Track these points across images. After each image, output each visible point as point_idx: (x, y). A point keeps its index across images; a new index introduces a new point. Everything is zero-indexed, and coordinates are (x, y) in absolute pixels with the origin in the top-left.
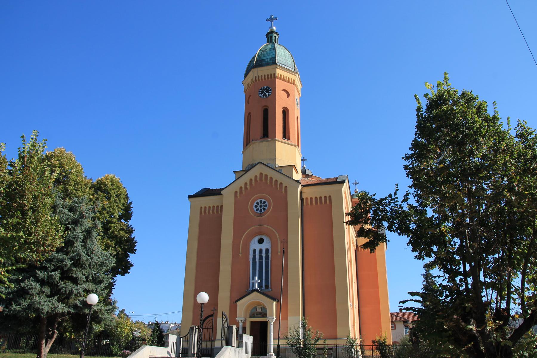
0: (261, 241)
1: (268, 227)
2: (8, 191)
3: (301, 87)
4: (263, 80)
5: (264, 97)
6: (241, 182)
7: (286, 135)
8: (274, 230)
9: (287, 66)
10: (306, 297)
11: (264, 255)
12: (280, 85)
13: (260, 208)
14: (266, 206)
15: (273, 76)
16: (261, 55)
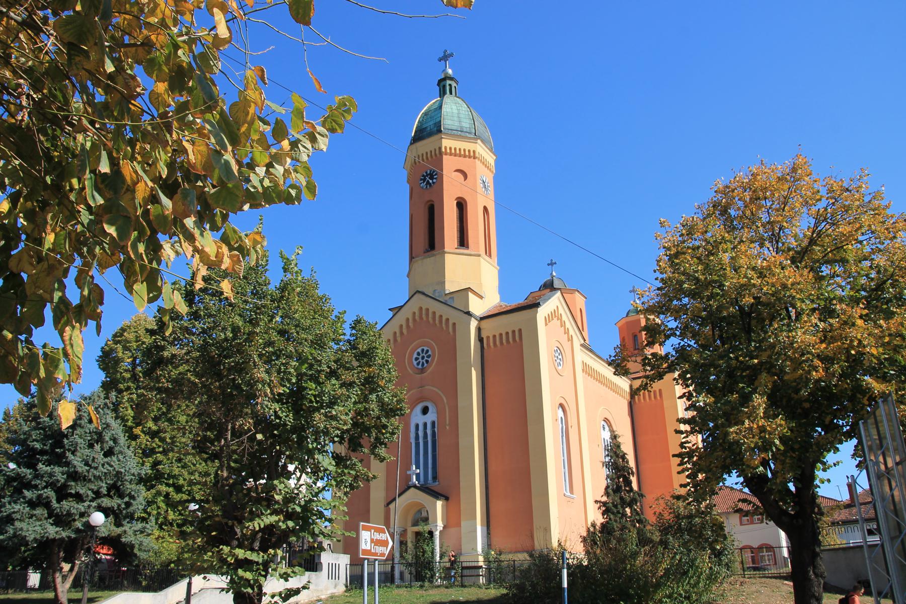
0: (425, 411)
3: (495, 158)
7: (463, 241)
8: (440, 392)
11: (429, 432)
12: (449, 164)
13: (421, 361)
14: (429, 356)
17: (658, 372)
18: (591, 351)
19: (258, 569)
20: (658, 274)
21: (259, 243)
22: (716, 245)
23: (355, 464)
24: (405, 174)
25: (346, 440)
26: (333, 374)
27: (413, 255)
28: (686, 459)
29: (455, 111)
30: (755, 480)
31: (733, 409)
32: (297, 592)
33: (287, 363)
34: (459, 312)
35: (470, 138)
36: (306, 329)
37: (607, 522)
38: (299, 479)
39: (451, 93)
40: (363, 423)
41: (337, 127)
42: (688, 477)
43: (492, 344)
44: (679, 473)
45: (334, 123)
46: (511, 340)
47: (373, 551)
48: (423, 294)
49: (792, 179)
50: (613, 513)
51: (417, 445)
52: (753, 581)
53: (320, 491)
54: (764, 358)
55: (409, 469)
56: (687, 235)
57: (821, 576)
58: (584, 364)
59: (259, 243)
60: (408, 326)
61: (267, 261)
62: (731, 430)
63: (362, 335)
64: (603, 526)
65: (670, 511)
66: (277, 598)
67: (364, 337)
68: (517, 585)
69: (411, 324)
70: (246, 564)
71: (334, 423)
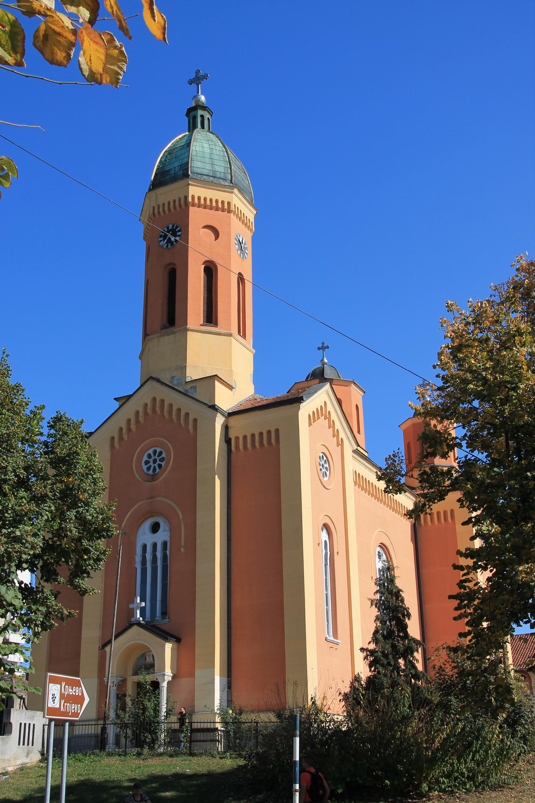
0: (155, 528)
2: (488, 657)
3: (255, 212)
4: (167, 212)
5: (167, 246)
6: (120, 421)
8: (175, 506)
9: (214, 177)
11: (159, 555)
14: (162, 460)
15: (182, 202)
16: (165, 160)
17: (438, 490)
20: (438, 371)
23: (47, 598)
24: (140, 229)
25: (39, 566)
26: (22, 483)
27: (148, 332)
28: (466, 602)
29: (207, 151)
31: (525, 542)
37: (374, 676)
39: (203, 127)
42: (467, 624)
43: (241, 447)
44: (455, 619)
48: (158, 381)
50: (383, 666)
55: (133, 601)
56: (474, 324)
58: (357, 476)
63: (62, 436)
64: (370, 680)
67: (65, 438)
68: (257, 754)
69: (141, 419)
71: (17, 546)
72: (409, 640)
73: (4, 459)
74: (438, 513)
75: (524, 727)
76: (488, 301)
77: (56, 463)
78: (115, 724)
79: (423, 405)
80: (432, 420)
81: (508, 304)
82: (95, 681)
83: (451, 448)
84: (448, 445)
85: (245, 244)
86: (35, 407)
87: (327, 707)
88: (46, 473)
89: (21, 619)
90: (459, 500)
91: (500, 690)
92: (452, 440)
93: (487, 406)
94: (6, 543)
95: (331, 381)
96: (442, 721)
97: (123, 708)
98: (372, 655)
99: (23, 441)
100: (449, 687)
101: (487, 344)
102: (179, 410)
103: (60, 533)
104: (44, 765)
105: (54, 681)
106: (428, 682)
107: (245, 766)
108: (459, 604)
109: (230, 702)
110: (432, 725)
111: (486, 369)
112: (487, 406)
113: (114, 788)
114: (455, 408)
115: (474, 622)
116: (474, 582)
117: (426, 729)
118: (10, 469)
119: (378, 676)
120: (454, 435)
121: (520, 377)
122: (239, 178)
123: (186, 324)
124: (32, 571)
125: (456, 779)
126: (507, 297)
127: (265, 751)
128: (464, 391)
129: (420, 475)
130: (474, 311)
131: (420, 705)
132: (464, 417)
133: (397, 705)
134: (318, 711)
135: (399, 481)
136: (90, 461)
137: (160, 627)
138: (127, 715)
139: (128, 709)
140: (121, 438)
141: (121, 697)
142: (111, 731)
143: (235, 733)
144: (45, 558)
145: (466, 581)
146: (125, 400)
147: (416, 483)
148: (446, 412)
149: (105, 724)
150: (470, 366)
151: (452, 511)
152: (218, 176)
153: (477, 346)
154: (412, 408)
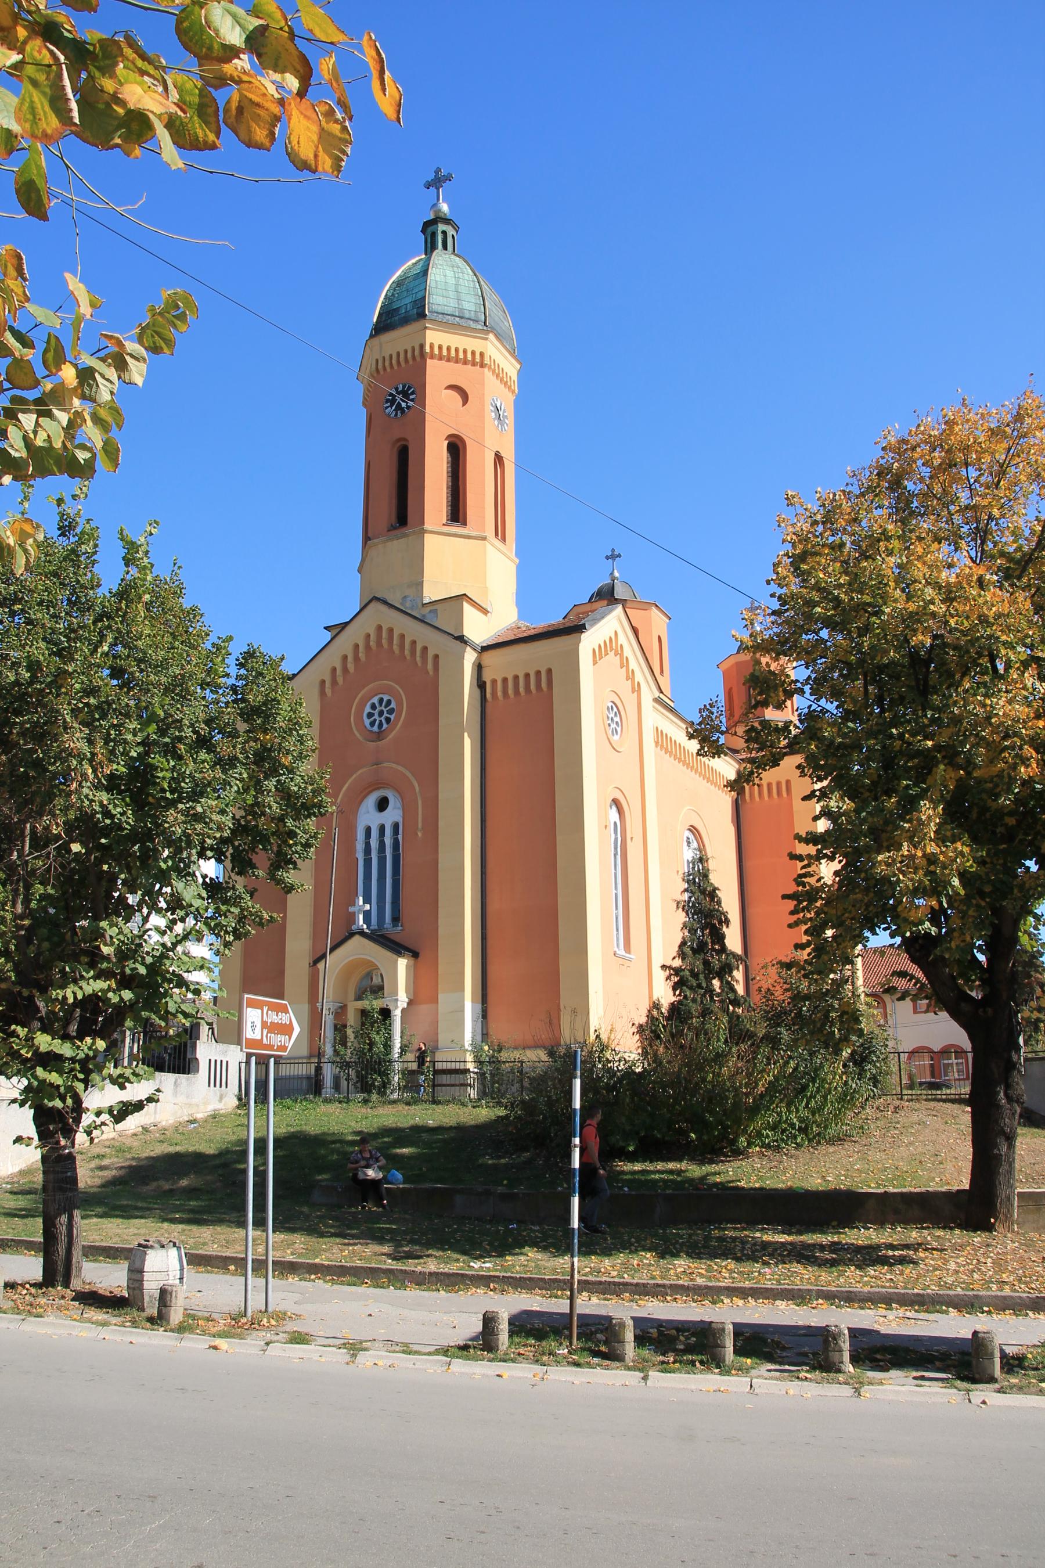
0: (382, 804)
1: (394, 766)
2: (832, 976)
3: (518, 366)
4: (396, 367)
5: (396, 415)
6: (332, 658)
7: (457, 513)
9: (461, 317)
10: (490, 942)
11: (388, 841)
15: (417, 353)
16: (393, 295)
17: (771, 753)
18: (671, 710)
19: (72, 1070)
20: (774, 588)
21: (29, 536)
22: (874, 541)
24: (358, 391)
25: (228, 854)
26: (203, 742)
27: (370, 535)
28: (805, 904)
29: (451, 281)
30: (920, 941)
31: (886, 822)
32: (139, 1106)
33: (122, 725)
34: (446, 636)
35: (476, 330)
36: (157, 666)
37: (680, 1002)
38: (146, 920)
39: (445, 247)
40: (257, 826)
41: (163, 345)
42: (806, 932)
43: (500, 694)
44: (790, 926)
45: (157, 338)
46: (533, 687)
47: (265, 1041)
48: (385, 602)
49: (1015, 433)
50: (691, 988)
51: (368, 862)
52: (917, 1105)
53: (179, 942)
54: (943, 740)
56: (823, 523)
57: (1018, 1101)
58: (660, 735)
59: (29, 536)
60: (356, 658)
61: (96, 546)
62: (879, 859)
63: (256, 677)
64: (674, 1008)
65: (786, 986)
66: (105, 1117)
67: (261, 680)
68: (523, 1102)
70: (51, 1060)
71: (199, 827)
72: (727, 955)
73: (178, 709)
74: (769, 785)
75: (875, 1066)
76: (843, 491)
77: (249, 714)
78: (333, 1062)
79: (751, 636)
80: (764, 656)
81: (870, 496)
82: (305, 1007)
83: (789, 695)
84: (785, 691)
85: (504, 411)
86: (219, 638)
87: (615, 1042)
88: (235, 729)
89: (206, 924)
90: (799, 767)
91: (846, 1017)
92: (790, 684)
93: (840, 637)
94: (184, 822)
95: (623, 602)
96: (768, 1059)
97: (344, 1042)
98: (676, 974)
99: (203, 685)
100: (778, 1016)
101: (841, 552)
102: (414, 643)
103: (254, 810)
104: (242, 1112)
105: (252, 1004)
106: (750, 1009)
107: (507, 1117)
108: (795, 906)
109: (485, 1036)
110: (755, 1064)
111: (840, 586)
112: (840, 637)
113: (334, 1142)
114: (796, 641)
115: (815, 930)
116: (816, 877)
117: (747, 1069)
118: (187, 723)
119: (685, 1002)
120: (793, 678)
121: (885, 598)
122: (497, 319)
123: (423, 523)
124: (219, 861)
125: (783, 1131)
126: (869, 487)
127: (533, 1098)
128: (809, 617)
129: (746, 732)
130: (824, 505)
131: (739, 1039)
132: (808, 653)
133: (709, 1040)
134: (604, 1048)
135: (717, 740)
136: (295, 712)
137: (392, 937)
138: (349, 1051)
139: (349, 1044)
140: (334, 682)
141: (340, 1028)
142: (328, 1072)
143: (492, 1075)
144: (236, 843)
145: (805, 875)
146: (338, 630)
147: (740, 744)
148: (782, 646)
149: (319, 1063)
150: (817, 583)
151: (788, 782)
152: (467, 316)
153: (827, 554)
154: (736, 639)
